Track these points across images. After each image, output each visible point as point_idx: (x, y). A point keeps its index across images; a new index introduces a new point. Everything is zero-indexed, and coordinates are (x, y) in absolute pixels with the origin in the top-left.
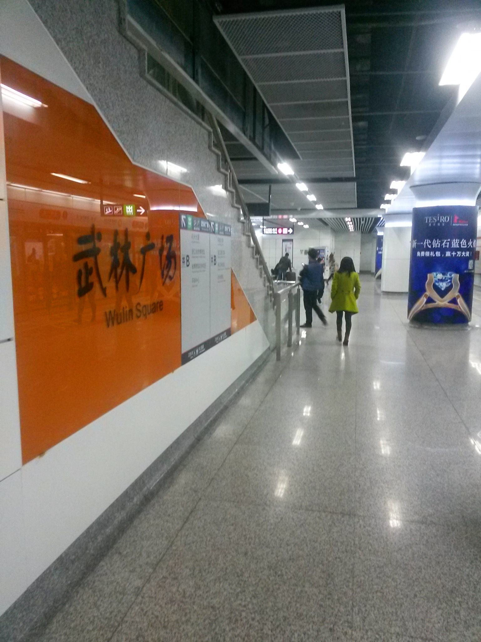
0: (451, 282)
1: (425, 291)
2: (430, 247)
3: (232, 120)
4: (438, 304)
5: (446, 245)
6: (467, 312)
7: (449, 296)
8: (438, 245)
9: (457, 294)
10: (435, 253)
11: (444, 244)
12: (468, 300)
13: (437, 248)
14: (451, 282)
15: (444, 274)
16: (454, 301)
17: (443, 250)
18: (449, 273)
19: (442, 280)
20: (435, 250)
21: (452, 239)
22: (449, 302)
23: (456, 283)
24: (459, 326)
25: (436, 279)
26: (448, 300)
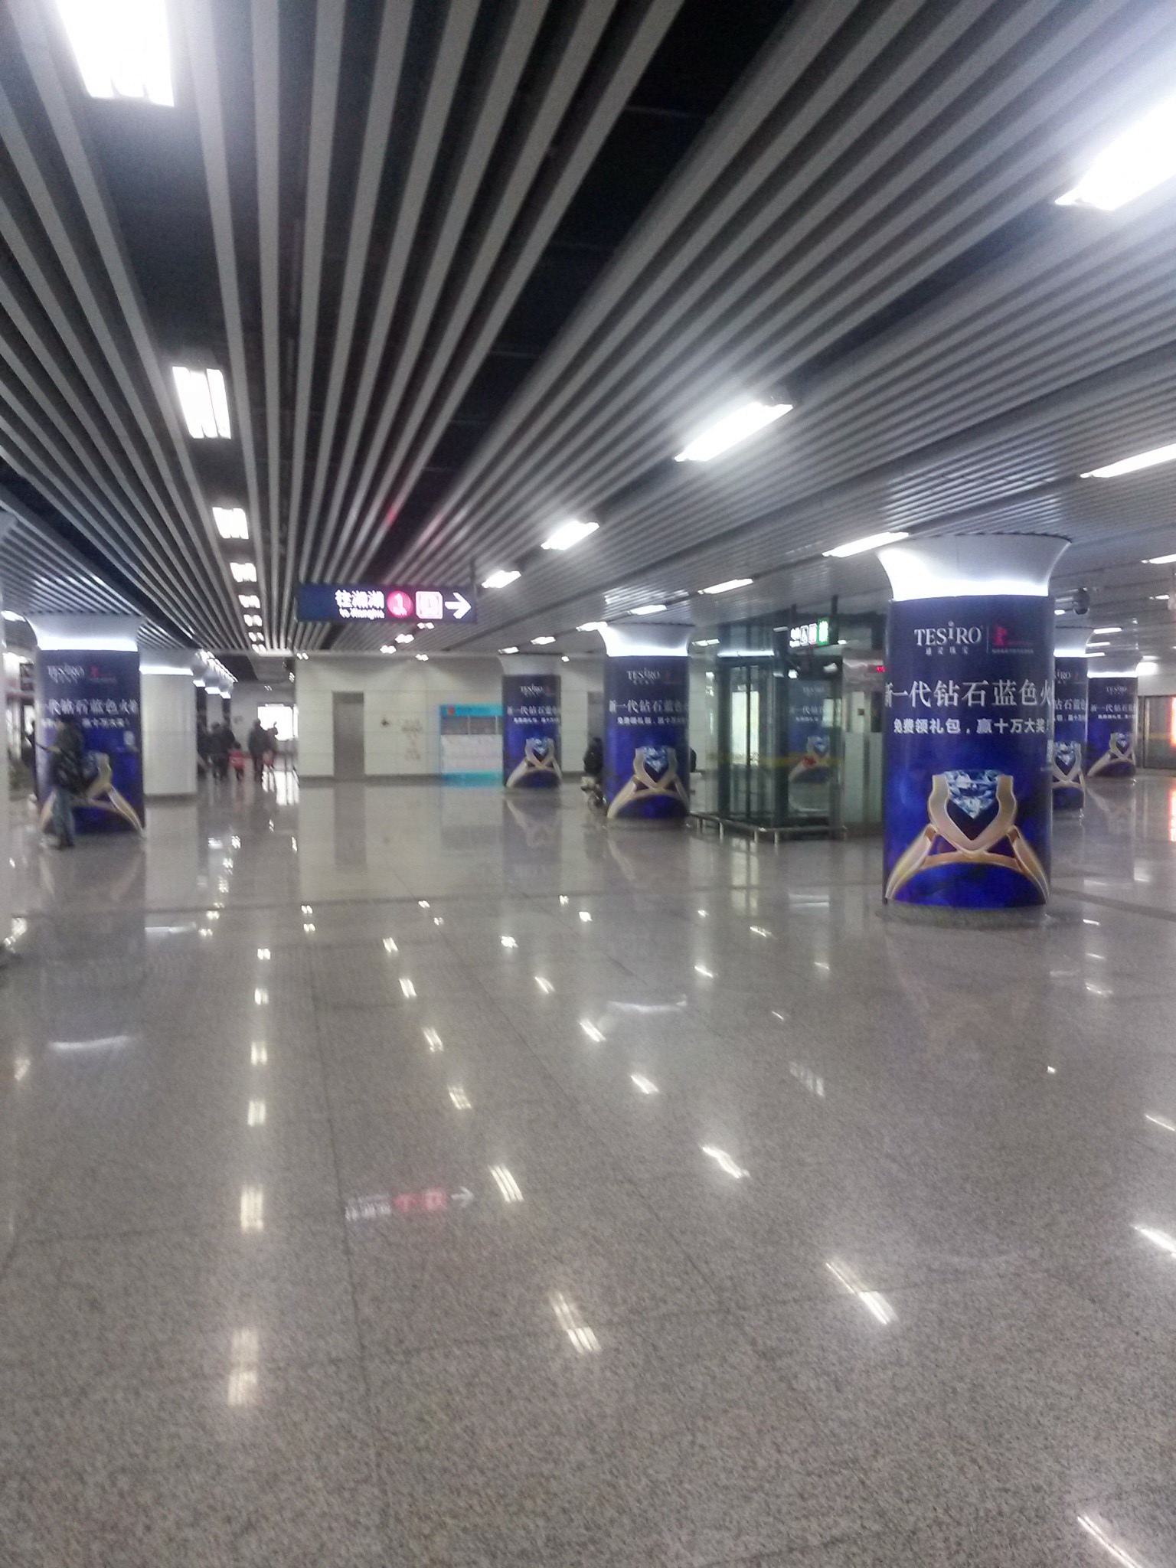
0: (993, 796)
1: (928, 821)
2: (928, 704)
3: (54, 809)
5: (976, 697)
6: (1036, 873)
7: (990, 834)
8: (951, 699)
9: (1010, 827)
10: (943, 725)
11: (969, 695)
12: (1038, 842)
13: (977, 707)
14: (993, 796)
15: (973, 777)
16: (1003, 847)
17: (539, 717)
18: (988, 772)
20: (531, 717)
21: (993, 678)
22: (990, 851)
23: (1009, 801)
24: (1017, 916)
26: (989, 845)
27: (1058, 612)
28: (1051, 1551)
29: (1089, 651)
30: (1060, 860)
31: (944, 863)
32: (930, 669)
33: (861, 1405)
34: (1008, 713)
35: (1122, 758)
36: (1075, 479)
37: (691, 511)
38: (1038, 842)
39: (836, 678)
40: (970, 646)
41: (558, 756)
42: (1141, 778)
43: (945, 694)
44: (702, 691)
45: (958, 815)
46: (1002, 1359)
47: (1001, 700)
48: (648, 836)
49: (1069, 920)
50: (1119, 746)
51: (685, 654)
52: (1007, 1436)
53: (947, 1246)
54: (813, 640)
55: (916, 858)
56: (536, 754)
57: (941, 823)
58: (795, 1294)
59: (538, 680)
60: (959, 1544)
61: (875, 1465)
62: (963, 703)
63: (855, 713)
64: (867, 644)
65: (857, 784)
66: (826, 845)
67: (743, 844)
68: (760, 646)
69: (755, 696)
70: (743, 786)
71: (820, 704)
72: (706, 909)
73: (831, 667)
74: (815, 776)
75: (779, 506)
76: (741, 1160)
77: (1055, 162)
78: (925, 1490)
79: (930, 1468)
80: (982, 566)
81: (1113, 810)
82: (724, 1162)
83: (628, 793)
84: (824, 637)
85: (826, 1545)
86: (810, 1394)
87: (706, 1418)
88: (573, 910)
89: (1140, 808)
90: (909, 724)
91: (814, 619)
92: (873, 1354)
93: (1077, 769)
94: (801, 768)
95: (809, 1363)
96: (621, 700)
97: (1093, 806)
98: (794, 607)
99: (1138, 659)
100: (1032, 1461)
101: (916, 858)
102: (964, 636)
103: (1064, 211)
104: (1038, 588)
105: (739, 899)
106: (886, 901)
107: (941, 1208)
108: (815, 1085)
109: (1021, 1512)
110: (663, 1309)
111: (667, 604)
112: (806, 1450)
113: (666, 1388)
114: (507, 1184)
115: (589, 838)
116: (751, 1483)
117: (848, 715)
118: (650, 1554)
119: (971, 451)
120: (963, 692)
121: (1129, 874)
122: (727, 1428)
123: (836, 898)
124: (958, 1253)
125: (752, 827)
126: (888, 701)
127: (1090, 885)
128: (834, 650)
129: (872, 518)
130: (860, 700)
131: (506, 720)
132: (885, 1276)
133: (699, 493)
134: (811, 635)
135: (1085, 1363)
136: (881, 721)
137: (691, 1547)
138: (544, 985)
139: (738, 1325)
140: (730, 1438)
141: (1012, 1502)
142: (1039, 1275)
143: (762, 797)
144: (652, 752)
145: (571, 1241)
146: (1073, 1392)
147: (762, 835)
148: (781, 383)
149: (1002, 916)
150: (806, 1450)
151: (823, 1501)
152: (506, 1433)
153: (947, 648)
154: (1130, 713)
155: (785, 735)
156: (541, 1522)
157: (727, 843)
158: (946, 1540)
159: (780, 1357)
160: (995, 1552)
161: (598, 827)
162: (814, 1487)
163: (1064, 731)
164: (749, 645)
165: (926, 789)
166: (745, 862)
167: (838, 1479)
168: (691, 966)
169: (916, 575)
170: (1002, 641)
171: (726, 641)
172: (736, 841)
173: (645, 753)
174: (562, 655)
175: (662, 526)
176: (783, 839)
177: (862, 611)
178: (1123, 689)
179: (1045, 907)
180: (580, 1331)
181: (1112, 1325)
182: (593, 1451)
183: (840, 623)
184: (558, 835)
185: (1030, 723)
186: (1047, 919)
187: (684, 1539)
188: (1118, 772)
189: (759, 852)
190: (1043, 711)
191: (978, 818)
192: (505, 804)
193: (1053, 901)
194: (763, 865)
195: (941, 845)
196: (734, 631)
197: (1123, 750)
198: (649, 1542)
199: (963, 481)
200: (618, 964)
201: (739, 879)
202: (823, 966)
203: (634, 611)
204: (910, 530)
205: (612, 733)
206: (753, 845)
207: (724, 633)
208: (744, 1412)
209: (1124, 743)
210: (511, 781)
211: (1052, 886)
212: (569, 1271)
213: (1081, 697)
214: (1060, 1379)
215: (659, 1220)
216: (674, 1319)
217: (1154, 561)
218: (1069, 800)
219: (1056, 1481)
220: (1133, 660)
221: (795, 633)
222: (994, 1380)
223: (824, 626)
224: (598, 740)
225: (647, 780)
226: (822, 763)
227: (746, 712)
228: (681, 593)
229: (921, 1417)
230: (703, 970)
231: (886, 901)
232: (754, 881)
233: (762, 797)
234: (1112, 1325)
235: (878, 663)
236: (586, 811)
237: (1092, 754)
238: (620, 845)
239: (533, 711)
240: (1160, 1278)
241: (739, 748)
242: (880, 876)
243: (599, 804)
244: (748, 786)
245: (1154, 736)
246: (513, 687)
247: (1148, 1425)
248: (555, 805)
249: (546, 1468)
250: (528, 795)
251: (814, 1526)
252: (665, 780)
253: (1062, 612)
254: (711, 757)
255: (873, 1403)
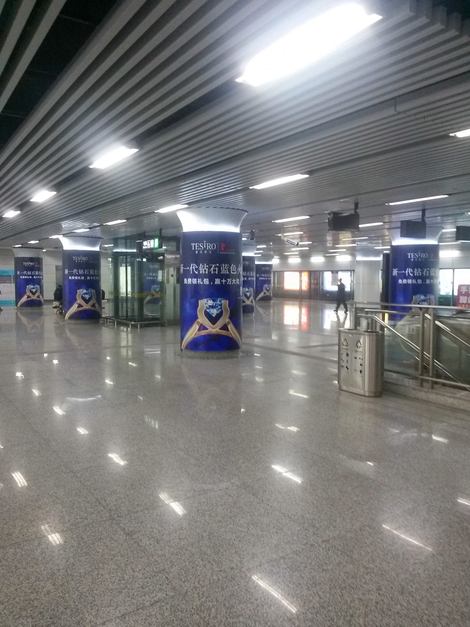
0: (221, 308)
2: (197, 273)
4: (210, 331)
5: (214, 270)
6: (237, 337)
7: (220, 323)
8: (205, 271)
9: (228, 320)
10: (202, 281)
11: (212, 269)
12: (237, 326)
14: (221, 308)
16: (225, 328)
17: (32, 276)
18: (219, 299)
19: (33, 288)
20: (29, 276)
21: (221, 263)
22: (220, 329)
23: (226, 309)
24: (230, 353)
25: (207, 306)
26: (220, 327)
27: (243, 239)
28: (236, 590)
29: (255, 254)
30: (246, 332)
31: (203, 334)
32: (197, 259)
33: (167, 547)
34: (227, 276)
35: (268, 294)
36: (247, 189)
37: (97, 189)
38: (237, 326)
39: (162, 261)
40: (212, 250)
41: (42, 292)
42: (275, 301)
43: (203, 269)
44: (106, 267)
45: (208, 315)
46: (220, 521)
47: (224, 271)
48: (84, 327)
49: (249, 354)
50: (267, 289)
51: (98, 250)
52: (222, 550)
53: (201, 481)
54: (152, 246)
55: (193, 332)
56: (31, 292)
57: (202, 319)
58: (142, 508)
59: (31, 259)
60: (203, 594)
61: (172, 570)
62: (210, 272)
63: (170, 276)
64: (174, 249)
65: (171, 305)
66: (159, 328)
67: (125, 329)
68: (131, 248)
69: (129, 268)
70: (125, 305)
71: (156, 271)
72: (110, 356)
73: (161, 257)
74: (154, 301)
75: (137, 190)
76: (122, 457)
77: (233, 66)
78: (191, 576)
79: (193, 567)
80: (216, 220)
81: (265, 313)
82: (116, 459)
83: (74, 309)
84: (157, 245)
85: (152, 605)
86: (147, 547)
87: (103, 563)
88: (50, 360)
89: (274, 312)
90: (190, 280)
91: (152, 237)
92: (172, 527)
93: (252, 298)
94: (149, 298)
95: (146, 535)
96: (70, 269)
97: (258, 311)
98: (144, 232)
99: (272, 257)
100: (230, 558)
101: (193, 333)
102: (210, 247)
103: (239, 84)
104: (235, 229)
105: (124, 352)
106: (182, 350)
107: (199, 467)
108: (155, 424)
109: (226, 578)
110: (86, 522)
111: (90, 228)
112: (144, 569)
113: (87, 553)
114: (19, 479)
115: (57, 328)
116: (122, 585)
117: (167, 277)
118: (78, 623)
119: (209, 175)
120: (210, 268)
121: (270, 337)
122: (112, 566)
123: (162, 350)
124: (205, 484)
125: (129, 322)
126: (182, 271)
127: (257, 341)
128: (161, 250)
129: (174, 198)
130: (172, 271)
131: (16, 277)
132: (177, 496)
133: (100, 182)
134: (152, 244)
135: (250, 518)
136: (180, 280)
137: (96, 616)
138: (36, 392)
139: (118, 524)
140: (114, 569)
141: (223, 575)
142: (234, 488)
143: (133, 310)
144: (85, 291)
145: (45, 500)
146: (246, 530)
147: (132, 325)
148: (132, 140)
149: (225, 354)
150: (144, 569)
151: (151, 587)
152: (14, 584)
153: (203, 251)
154: (270, 277)
155: (142, 284)
156: (29, 620)
157: (118, 329)
158: (198, 593)
159: (135, 534)
160: (216, 594)
161: (61, 323)
162: (148, 583)
163: (246, 284)
164: (126, 247)
165: (196, 306)
166: (126, 337)
167: (157, 578)
168: (103, 379)
169: (192, 222)
170: (223, 250)
171: (116, 245)
172: (122, 328)
173: (81, 292)
174: (43, 248)
175: (85, 195)
176: (142, 326)
177: (171, 235)
178: (267, 268)
179: (240, 350)
180: (53, 535)
181: (260, 503)
182: (54, 585)
183: (163, 239)
184: (42, 327)
185: (234, 280)
186: (241, 354)
187: (93, 614)
188: (267, 299)
189: (132, 332)
190: (238, 276)
191: (215, 317)
192: (17, 314)
193: (243, 347)
194: (133, 337)
195: (202, 327)
196: (119, 241)
197: (268, 291)
198: (78, 618)
199: (208, 186)
200: (68, 381)
201: (124, 343)
202: (158, 377)
203: (75, 231)
204: (189, 204)
205: (67, 283)
206: (129, 329)
207: (116, 242)
208: (119, 558)
209: (268, 288)
210: (19, 305)
211: (243, 342)
212: (44, 512)
213: (253, 271)
214: (241, 526)
215: (85, 486)
216: (90, 526)
217: (276, 221)
218: (248, 310)
219: (239, 564)
220: (270, 258)
221: (145, 243)
222: (218, 530)
223: (157, 240)
224: (60, 286)
225: (83, 303)
226: (158, 296)
227: (125, 275)
228: (96, 224)
229: (190, 548)
230: (109, 382)
231: (182, 350)
232: (130, 344)
233: (133, 310)
234: (260, 503)
235: (178, 256)
236: (55, 316)
237: (257, 293)
238: (71, 330)
239: (29, 273)
240: (276, 483)
241: (123, 290)
242: (180, 340)
243: (61, 313)
244: (127, 306)
245: (278, 286)
246: (19, 262)
247: (271, 537)
248: (41, 314)
249: (32, 596)
250: (28, 310)
251: (147, 597)
252: (91, 303)
253: (245, 239)
254: (110, 293)
255: (171, 546)
